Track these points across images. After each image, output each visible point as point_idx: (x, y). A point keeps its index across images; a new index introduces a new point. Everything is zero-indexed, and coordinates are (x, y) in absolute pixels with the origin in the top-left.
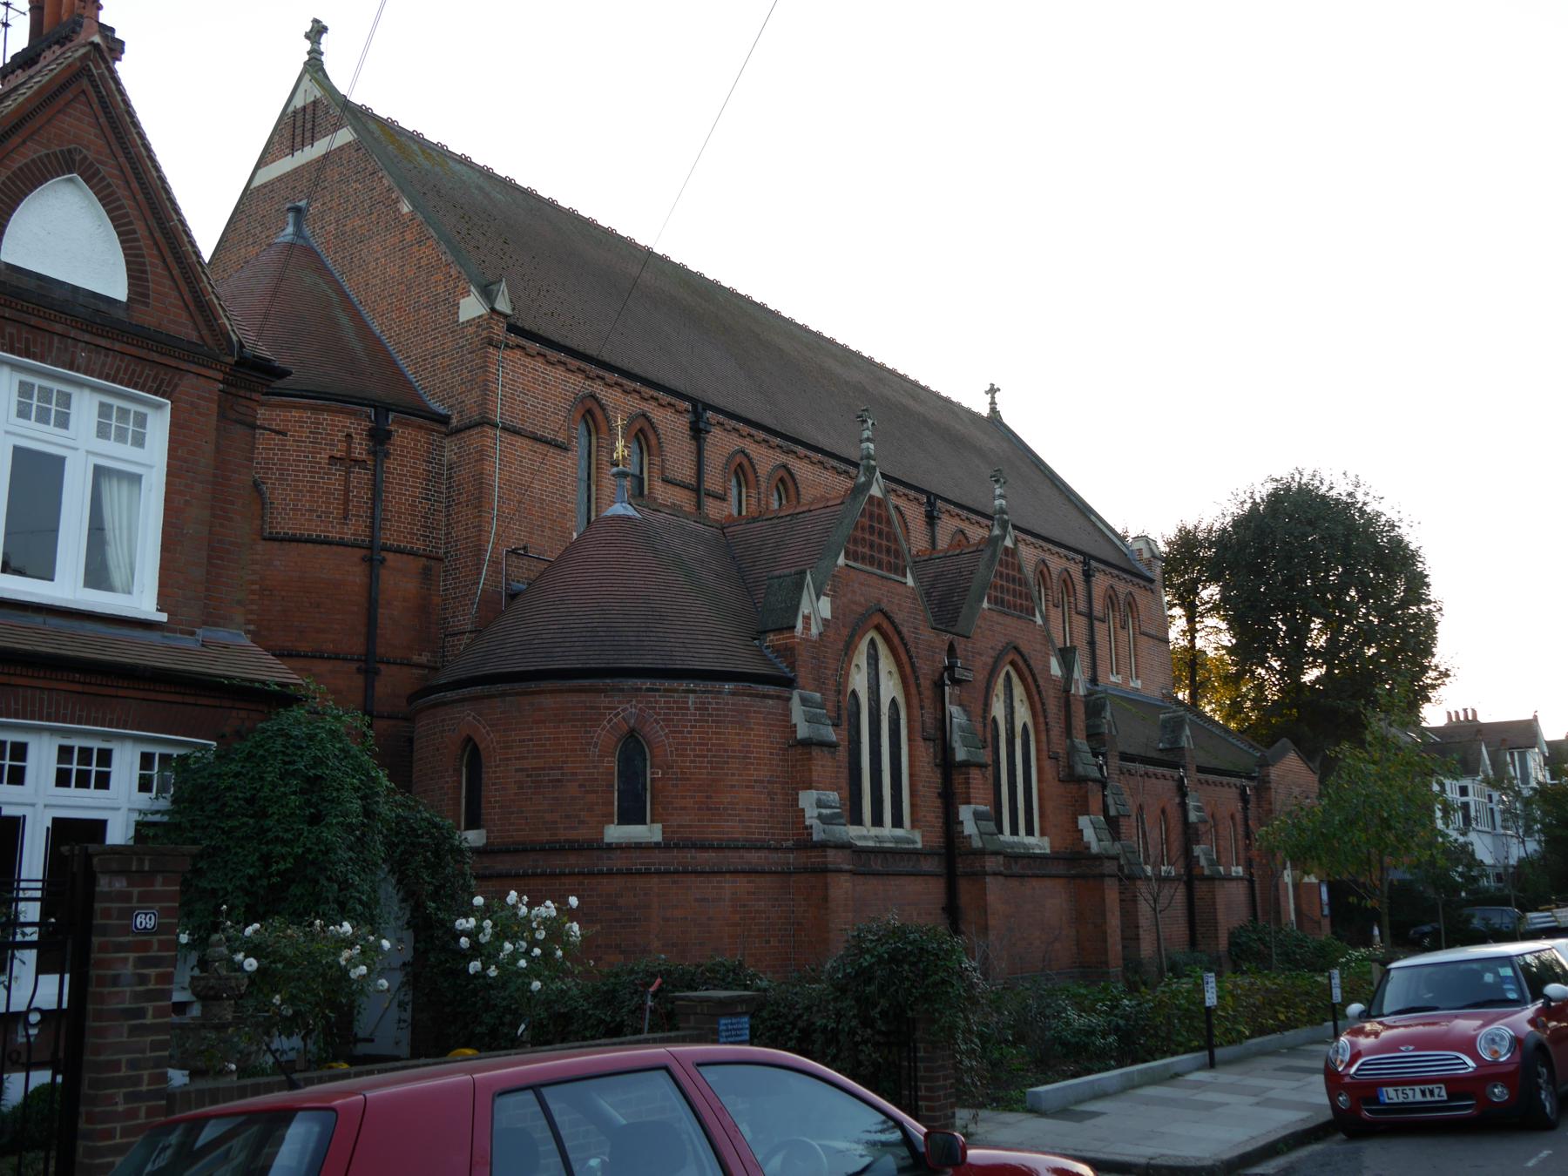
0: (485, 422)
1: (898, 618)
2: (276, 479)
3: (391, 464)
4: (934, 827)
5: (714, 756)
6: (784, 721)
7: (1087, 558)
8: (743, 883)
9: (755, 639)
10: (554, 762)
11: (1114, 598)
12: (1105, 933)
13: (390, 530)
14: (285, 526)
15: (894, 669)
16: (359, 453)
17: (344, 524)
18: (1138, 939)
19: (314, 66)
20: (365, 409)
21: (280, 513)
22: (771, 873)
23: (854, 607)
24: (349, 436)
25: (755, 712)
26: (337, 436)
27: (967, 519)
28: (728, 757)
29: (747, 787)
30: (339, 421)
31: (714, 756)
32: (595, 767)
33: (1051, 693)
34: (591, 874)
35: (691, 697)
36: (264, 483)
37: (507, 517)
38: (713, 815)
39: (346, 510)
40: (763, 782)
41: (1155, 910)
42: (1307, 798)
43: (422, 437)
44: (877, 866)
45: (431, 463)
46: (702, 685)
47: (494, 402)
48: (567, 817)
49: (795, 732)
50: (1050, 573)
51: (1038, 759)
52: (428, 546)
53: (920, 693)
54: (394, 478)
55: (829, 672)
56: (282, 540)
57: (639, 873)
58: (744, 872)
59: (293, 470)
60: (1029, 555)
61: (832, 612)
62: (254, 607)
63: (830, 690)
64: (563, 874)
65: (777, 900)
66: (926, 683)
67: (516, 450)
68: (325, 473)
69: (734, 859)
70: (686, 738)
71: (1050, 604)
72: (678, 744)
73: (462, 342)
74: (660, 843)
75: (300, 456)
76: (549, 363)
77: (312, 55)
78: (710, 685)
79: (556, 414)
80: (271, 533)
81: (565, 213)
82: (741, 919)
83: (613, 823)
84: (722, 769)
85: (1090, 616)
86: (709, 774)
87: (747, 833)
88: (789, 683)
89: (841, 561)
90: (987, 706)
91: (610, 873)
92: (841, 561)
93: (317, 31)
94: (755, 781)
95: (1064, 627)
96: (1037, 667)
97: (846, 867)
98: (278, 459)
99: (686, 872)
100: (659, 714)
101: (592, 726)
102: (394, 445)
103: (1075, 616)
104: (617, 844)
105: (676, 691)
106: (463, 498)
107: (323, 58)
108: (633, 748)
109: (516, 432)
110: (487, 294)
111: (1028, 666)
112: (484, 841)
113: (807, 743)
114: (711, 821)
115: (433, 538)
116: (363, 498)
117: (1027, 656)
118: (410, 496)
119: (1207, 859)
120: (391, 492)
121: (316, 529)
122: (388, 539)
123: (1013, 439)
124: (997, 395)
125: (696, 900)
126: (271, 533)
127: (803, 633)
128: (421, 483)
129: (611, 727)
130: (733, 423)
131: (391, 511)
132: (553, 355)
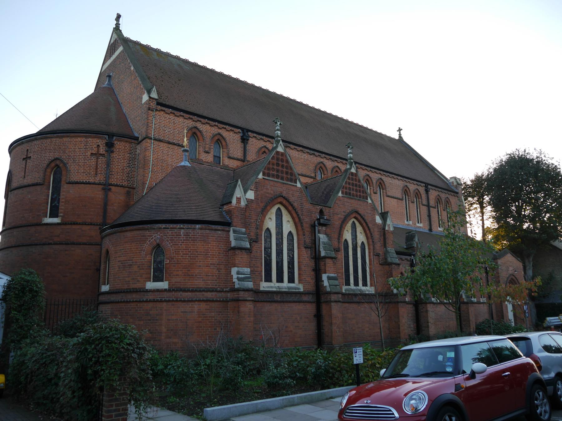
0: (147, 137)
1: (292, 199)
2: (72, 162)
3: (114, 155)
4: (310, 283)
5: (192, 254)
6: (227, 240)
7: (427, 185)
8: (203, 306)
9: (220, 208)
10: (130, 258)
11: (440, 199)
12: (399, 325)
13: (113, 178)
14: (74, 178)
15: (290, 220)
16: (102, 152)
17: (95, 177)
18: (428, 327)
19: (117, 29)
20: (104, 136)
21: (73, 174)
22: (217, 301)
23: (268, 195)
24: (98, 146)
25: (211, 236)
26: (94, 146)
27: (370, 170)
28: (198, 254)
29: (206, 266)
30: (95, 141)
31: (192, 254)
32: (144, 259)
33: (376, 230)
34: (140, 302)
35: (182, 231)
36: (68, 164)
37: (156, 172)
38: (190, 278)
39: (96, 172)
40: (214, 264)
41: (379, 316)
42: (515, 271)
43: (127, 145)
44: (278, 298)
45: (131, 154)
46: (186, 226)
47: (151, 130)
48: (133, 279)
49: (231, 244)
50: (409, 190)
51: (369, 256)
52: (129, 184)
53: (303, 229)
54: (115, 160)
55: (253, 221)
56: (73, 183)
57: (157, 301)
58: (203, 301)
59: (78, 159)
60: (362, 173)
61: (255, 197)
62: (63, 207)
63: (253, 228)
64: (130, 302)
65: (221, 312)
66: (307, 226)
67: (161, 148)
68: (89, 159)
69: (200, 295)
70: (180, 247)
71: (410, 202)
72: (176, 249)
73: (143, 110)
74: (166, 289)
75: (125, 161)
76: (176, 116)
77: (117, 25)
78: (190, 226)
79: (179, 134)
80: (69, 181)
81: (249, 85)
82: (202, 320)
83: (150, 281)
84: (195, 259)
85: (428, 206)
86: (189, 261)
87: (206, 285)
88: (229, 224)
89: (261, 176)
90: (340, 235)
91: (147, 301)
92: (261, 176)
93: (119, 17)
94: (211, 264)
95: (417, 211)
96: (368, 219)
97: (250, 299)
98: (73, 155)
99: (177, 301)
100: (168, 238)
101: (144, 243)
102: (116, 148)
103: (421, 206)
104: (150, 289)
105: (175, 228)
106: (140, 166)
107: (120, 26)
108: (158, 249)
109: (160, 141)
110: (149, 92)
111: (363, 219)
112: (109, 289)
113: (234, 249)
114: (189, 280)
115: (131, 181)
116: (103, 167)
117: (362, 215)
118: (122, 166)
119: (465, 296)
120: (114, 165)
121: (85, 179)
122: (113, 182)
123: (407, 146)
124: (401, 131)
125: (182, 312)
126: (69, 181)
127: (236, 205)
128: (126, 161)
129: (150, 244)
130: (261, 137)
131: (114, 172)
132: (178, 113)
